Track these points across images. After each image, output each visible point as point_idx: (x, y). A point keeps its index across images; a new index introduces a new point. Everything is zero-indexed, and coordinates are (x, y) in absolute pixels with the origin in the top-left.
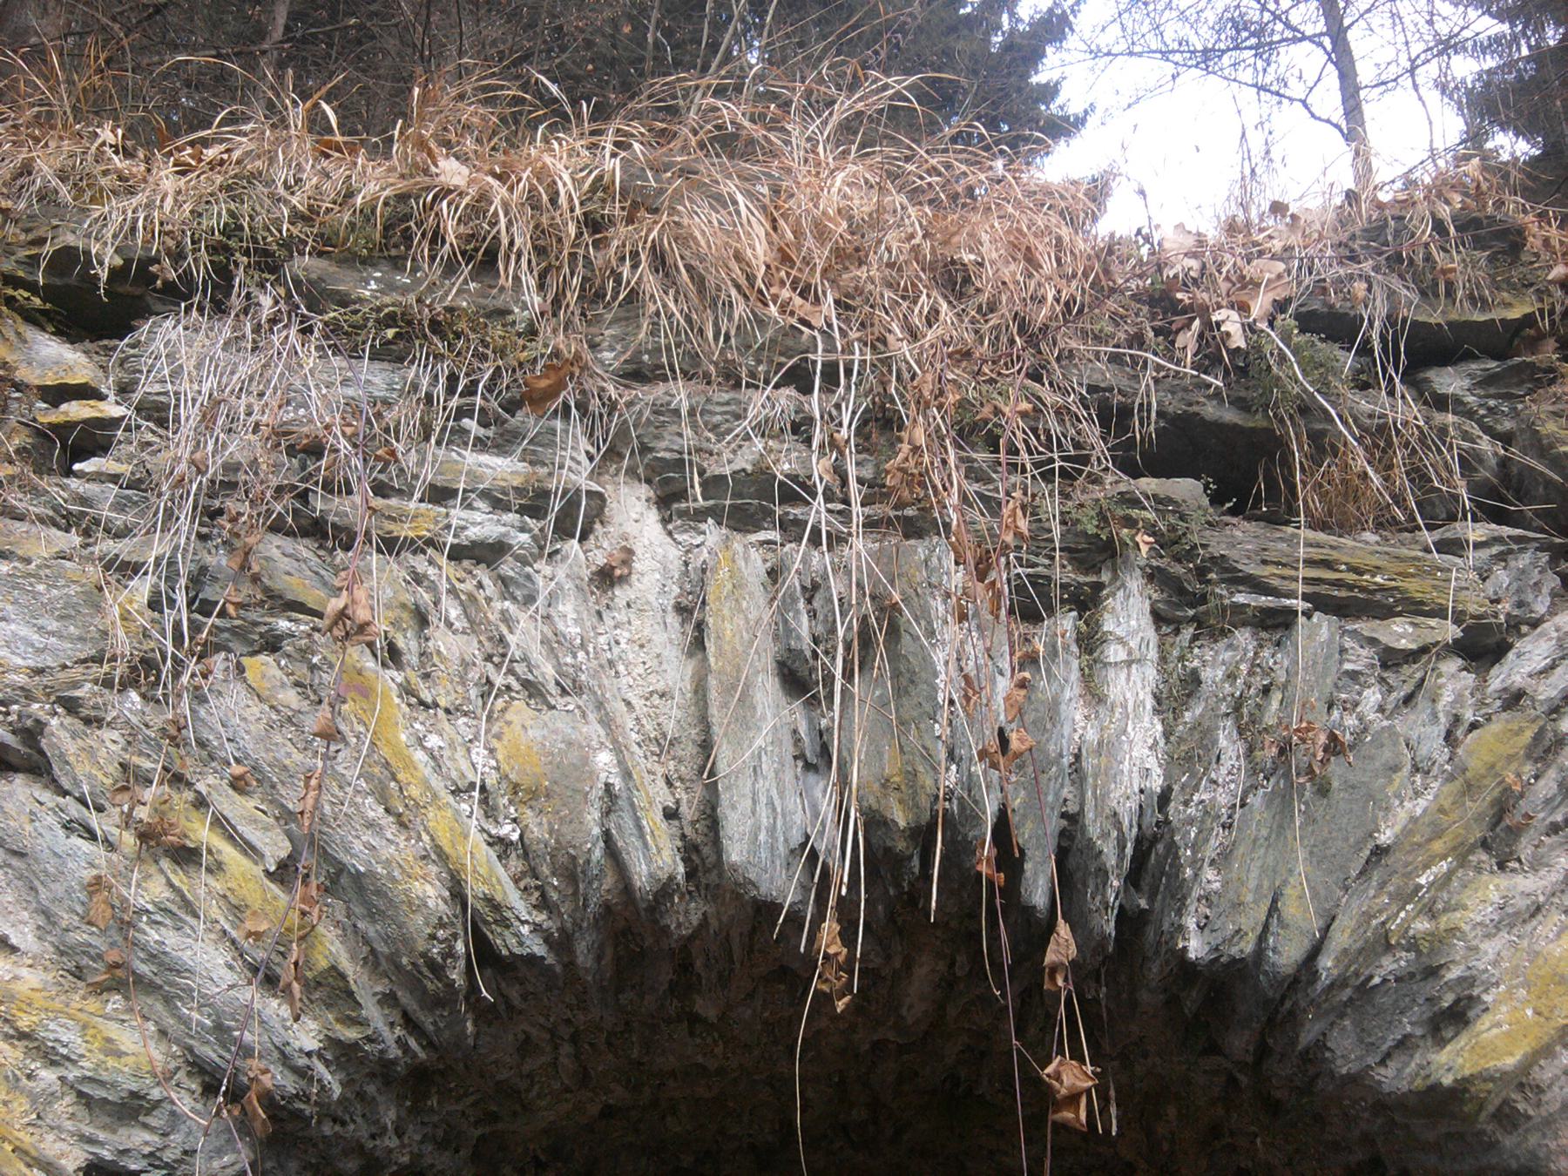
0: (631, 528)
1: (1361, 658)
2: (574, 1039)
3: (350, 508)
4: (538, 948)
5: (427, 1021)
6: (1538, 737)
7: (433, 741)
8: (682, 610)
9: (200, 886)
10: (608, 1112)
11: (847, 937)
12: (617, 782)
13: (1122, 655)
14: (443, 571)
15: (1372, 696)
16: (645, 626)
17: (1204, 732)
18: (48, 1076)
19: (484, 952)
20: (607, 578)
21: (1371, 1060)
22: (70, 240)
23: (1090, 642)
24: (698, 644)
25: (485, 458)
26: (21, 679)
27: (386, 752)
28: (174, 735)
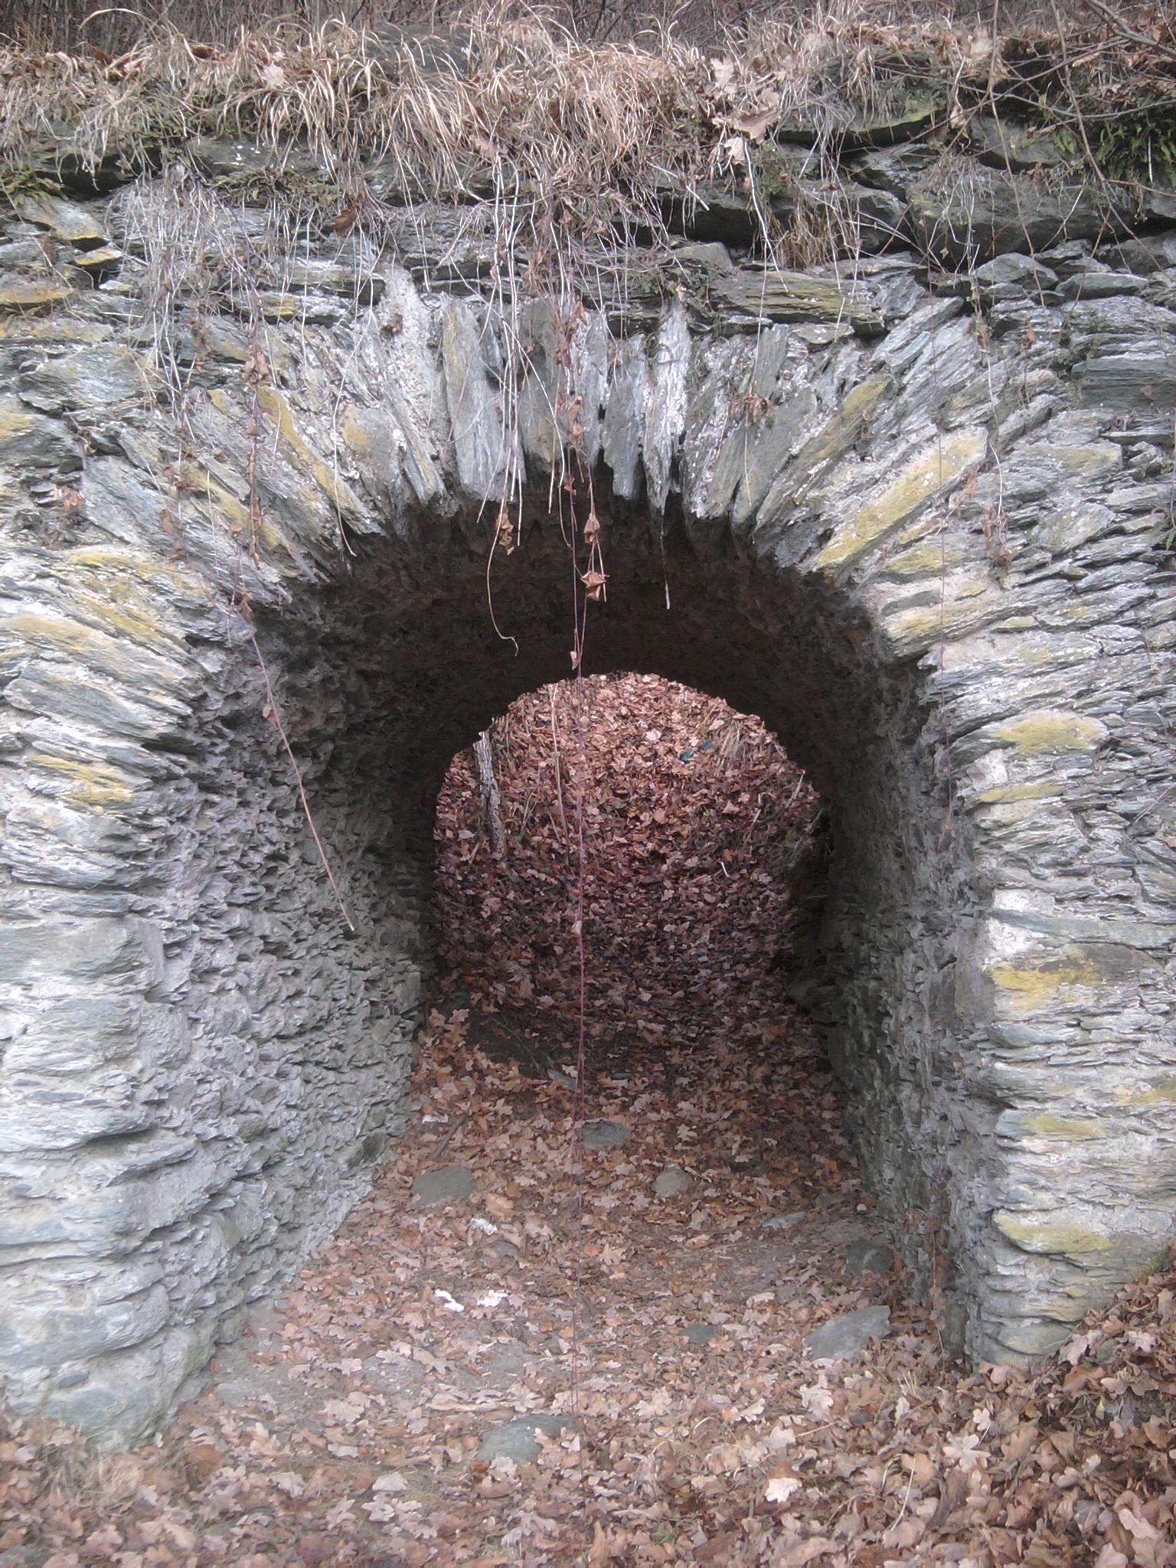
0: (400, 300)
1: (797, 348)
2: (406, 567)
3: (245, 299)
4: (376, 529)
5: (328, 566)
6: (889, 387)
7: (311, 430)
8: (432, 347)
9: (208, 508)
10: (436, 603)
11: (513, 519)
12: (405, 445)
13: (668, 358)
14: (301, 333)
15: (803, 370)
16: (412, 358)
17: (707, 402)
18: (161, 599)
19: (349, 532)
20: (389, 332)
21: (796, 560)
22: (70, 150)
23: (652, 349)
24: (440, 365)
25: (317, 264)
26: (101, 409)
27: (288, 437)
28: (182, 433)
